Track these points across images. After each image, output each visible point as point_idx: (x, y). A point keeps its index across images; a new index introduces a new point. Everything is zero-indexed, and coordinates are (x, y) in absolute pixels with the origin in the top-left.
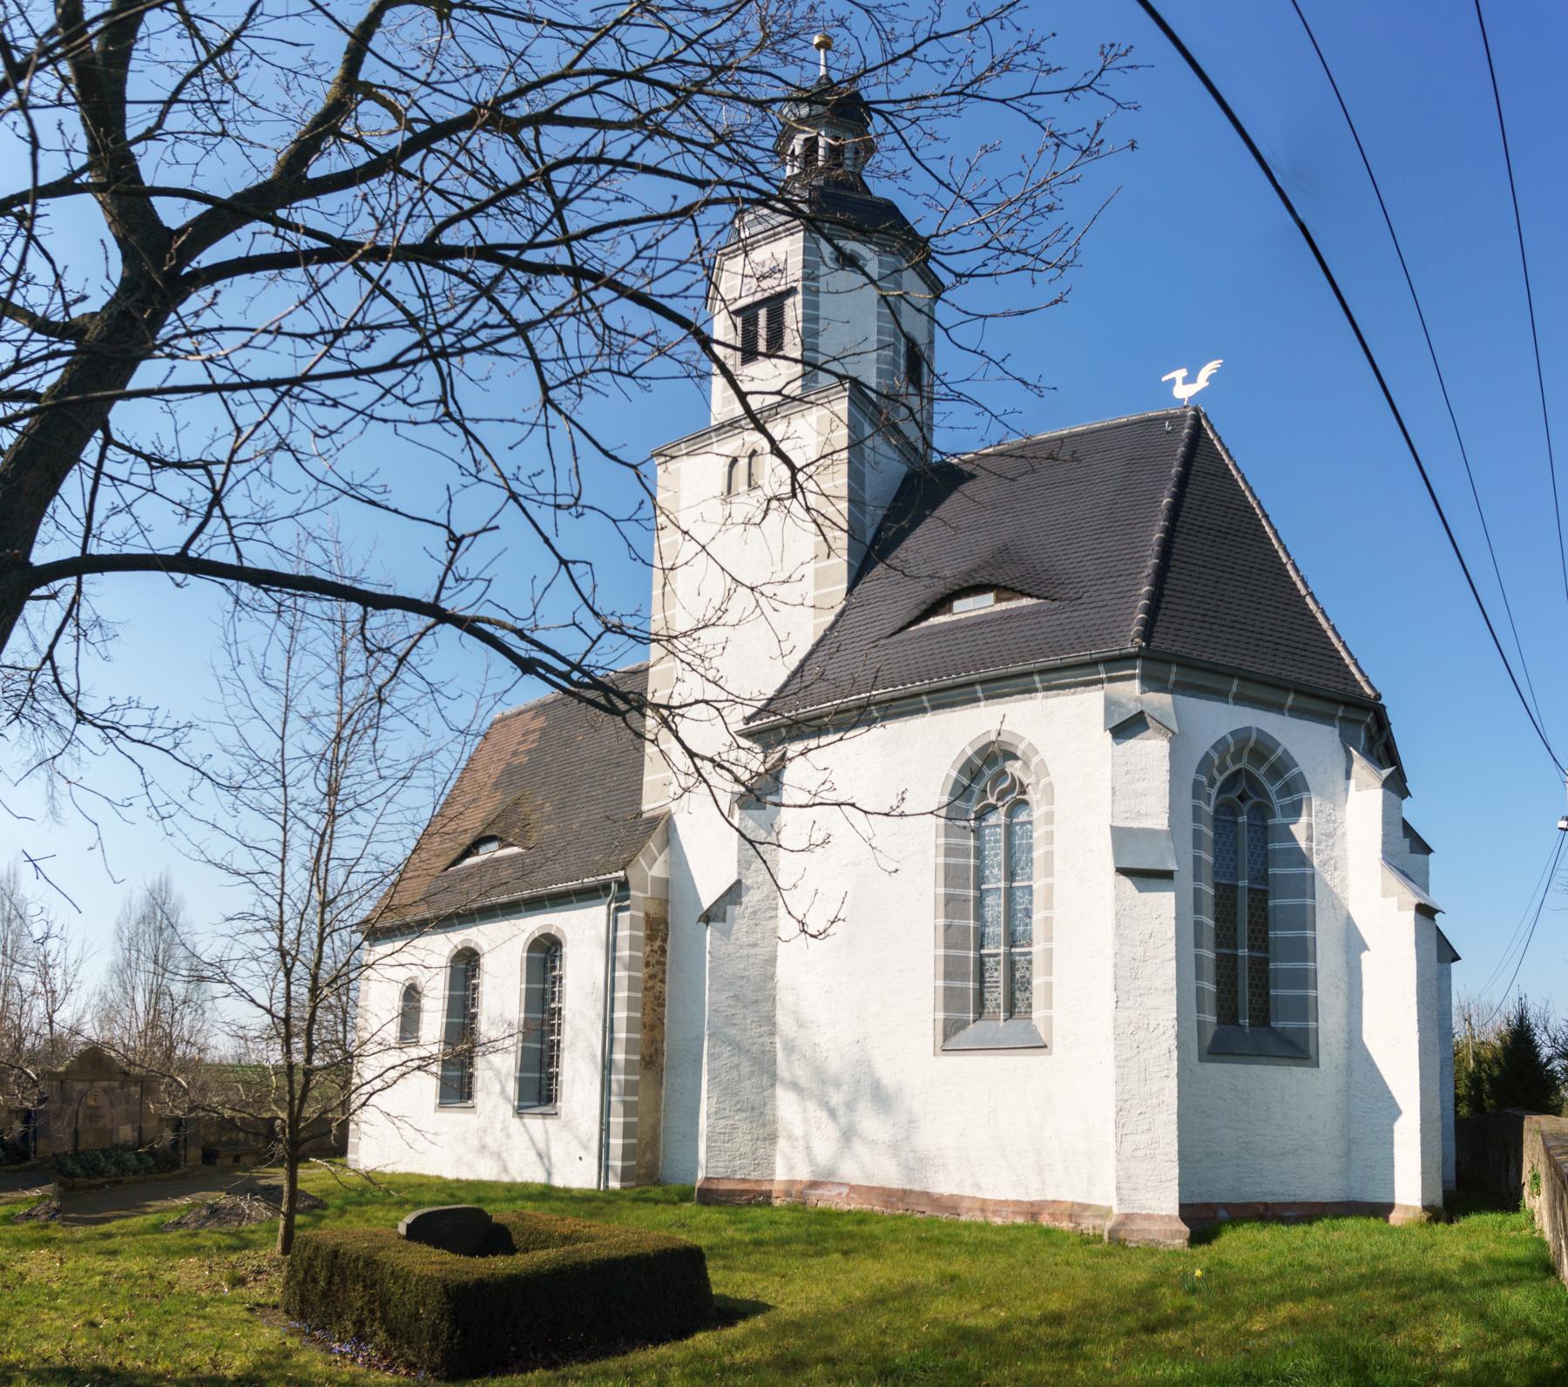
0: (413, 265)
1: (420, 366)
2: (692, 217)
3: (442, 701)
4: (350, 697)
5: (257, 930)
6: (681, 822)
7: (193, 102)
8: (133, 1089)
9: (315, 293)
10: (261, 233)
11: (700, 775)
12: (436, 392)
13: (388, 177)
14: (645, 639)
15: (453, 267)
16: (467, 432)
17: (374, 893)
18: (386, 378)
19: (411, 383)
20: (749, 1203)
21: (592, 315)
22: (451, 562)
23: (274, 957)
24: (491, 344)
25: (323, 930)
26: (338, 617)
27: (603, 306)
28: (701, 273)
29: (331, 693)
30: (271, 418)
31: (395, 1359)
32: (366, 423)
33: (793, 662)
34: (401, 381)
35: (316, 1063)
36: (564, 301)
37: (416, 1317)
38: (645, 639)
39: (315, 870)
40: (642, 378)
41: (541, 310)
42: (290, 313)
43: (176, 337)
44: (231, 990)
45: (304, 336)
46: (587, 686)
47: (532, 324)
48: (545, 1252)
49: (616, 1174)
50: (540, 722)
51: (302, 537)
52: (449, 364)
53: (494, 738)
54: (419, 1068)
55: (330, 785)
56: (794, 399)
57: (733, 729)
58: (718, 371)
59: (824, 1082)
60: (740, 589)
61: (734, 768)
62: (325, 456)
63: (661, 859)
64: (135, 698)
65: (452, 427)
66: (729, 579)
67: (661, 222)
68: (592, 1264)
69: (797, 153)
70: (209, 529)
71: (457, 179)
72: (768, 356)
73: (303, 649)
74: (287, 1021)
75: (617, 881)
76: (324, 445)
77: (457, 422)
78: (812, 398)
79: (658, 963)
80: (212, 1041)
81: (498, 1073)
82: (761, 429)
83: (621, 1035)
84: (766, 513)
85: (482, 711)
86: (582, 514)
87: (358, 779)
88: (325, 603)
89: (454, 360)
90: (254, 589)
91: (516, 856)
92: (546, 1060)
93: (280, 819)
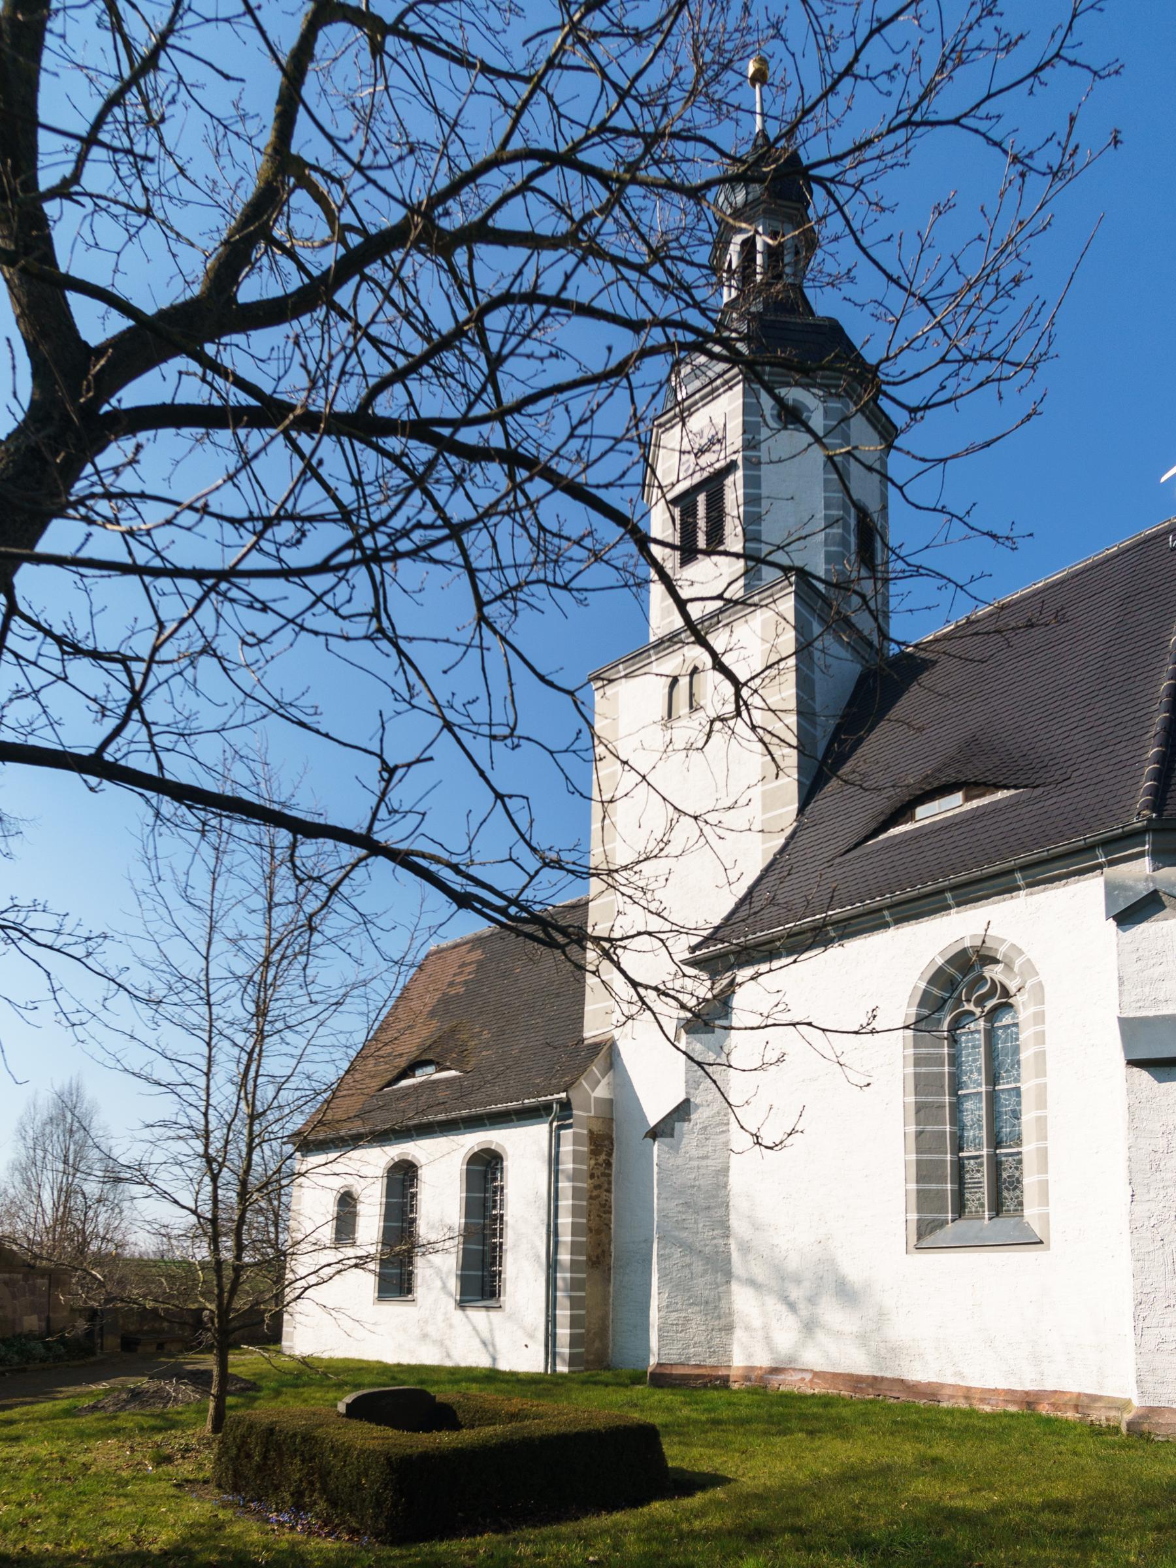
0: (345, 440)
1: (352, 570)
2: (627, 377)
3: (375, 932)
4: (279, 923)
5: (180, 1138)
6: (626, 1049)
7: (115, 150)
8: (39, 1281)
9: (244, 467)
10: (188, 374)
11: (644, 1003)
12: (368, 605)
13: (320, 313)
14: (584, 873)
15: (387, 447)
16: (400, 652)
17: (306, 1109)
18: (320, 583)
19: (343, 591)
20: (705, 1386)
21: (527, 514)
22: (384, 793)
23: (199, 1163)
24: (425, 548)
25: (252, 1140)
26: (266, 841)
27: (538, 501)
28: (638, 452)
29: (259, 918)
30: (196, 616)
31: (337, 1525)
32: (297, 634)
33: (741, 890)
34: (333, 588)
35: (246, 1260)
36: (499, 495)
37: (358, 1487)
38: (584, 873)
39: (243, 1085)
40: (578, 590)
41: (475, 507)
42: (218, 488)
43: (93, 496)
44: (152, 1191)
45: (232, 521)
46: (524, 921)
47: (466, 525)
48: (491, 1428)
49: (563, 1360)
50: (477, 955)
51: (228, 755)
52: (382, 571)
53: (429, 969)
54: (356, 1266)
55: (258, 1006)
56: (736, 603)
57: (677, 958)
58: (656, 577)
59: (783, 1279)
60: (683, 819)
61: (679, 996)
62: (254, 668)
63: (604, 1082)
64: (41, 901)
65: (385, 645)
66: (671, 809)
67: (595, 386)
68: (541, 1438)
69: (734, 266)
70: (127, 733)
71: (390, 322)
72: (708, 553)
73: (229, 871)
74: (214, 1221)
75: (559, 1101)
76: (252, 654)
77: (390, 640)
78: (756, 599)
79: (603, 1174)
80: (131, 1238)
81: (438, 1271)
82: (702, 642)
83: (566, 1237)
84: (709, 736)
85: (417, 943)
86: (518, 746)
87: (288, 1002)
88: (253, 827)
89: (388, 566)
90: (177, 804)
91: (454, 1078)
92: (488, 1260)
93: (205, 1036)
